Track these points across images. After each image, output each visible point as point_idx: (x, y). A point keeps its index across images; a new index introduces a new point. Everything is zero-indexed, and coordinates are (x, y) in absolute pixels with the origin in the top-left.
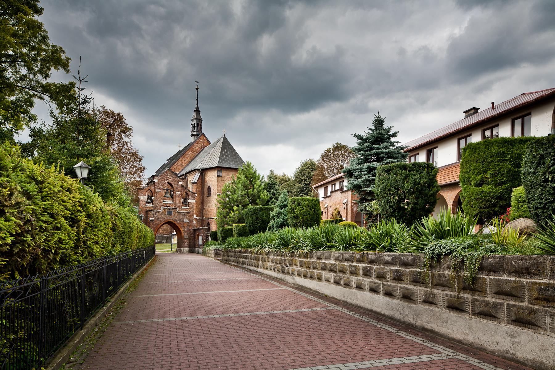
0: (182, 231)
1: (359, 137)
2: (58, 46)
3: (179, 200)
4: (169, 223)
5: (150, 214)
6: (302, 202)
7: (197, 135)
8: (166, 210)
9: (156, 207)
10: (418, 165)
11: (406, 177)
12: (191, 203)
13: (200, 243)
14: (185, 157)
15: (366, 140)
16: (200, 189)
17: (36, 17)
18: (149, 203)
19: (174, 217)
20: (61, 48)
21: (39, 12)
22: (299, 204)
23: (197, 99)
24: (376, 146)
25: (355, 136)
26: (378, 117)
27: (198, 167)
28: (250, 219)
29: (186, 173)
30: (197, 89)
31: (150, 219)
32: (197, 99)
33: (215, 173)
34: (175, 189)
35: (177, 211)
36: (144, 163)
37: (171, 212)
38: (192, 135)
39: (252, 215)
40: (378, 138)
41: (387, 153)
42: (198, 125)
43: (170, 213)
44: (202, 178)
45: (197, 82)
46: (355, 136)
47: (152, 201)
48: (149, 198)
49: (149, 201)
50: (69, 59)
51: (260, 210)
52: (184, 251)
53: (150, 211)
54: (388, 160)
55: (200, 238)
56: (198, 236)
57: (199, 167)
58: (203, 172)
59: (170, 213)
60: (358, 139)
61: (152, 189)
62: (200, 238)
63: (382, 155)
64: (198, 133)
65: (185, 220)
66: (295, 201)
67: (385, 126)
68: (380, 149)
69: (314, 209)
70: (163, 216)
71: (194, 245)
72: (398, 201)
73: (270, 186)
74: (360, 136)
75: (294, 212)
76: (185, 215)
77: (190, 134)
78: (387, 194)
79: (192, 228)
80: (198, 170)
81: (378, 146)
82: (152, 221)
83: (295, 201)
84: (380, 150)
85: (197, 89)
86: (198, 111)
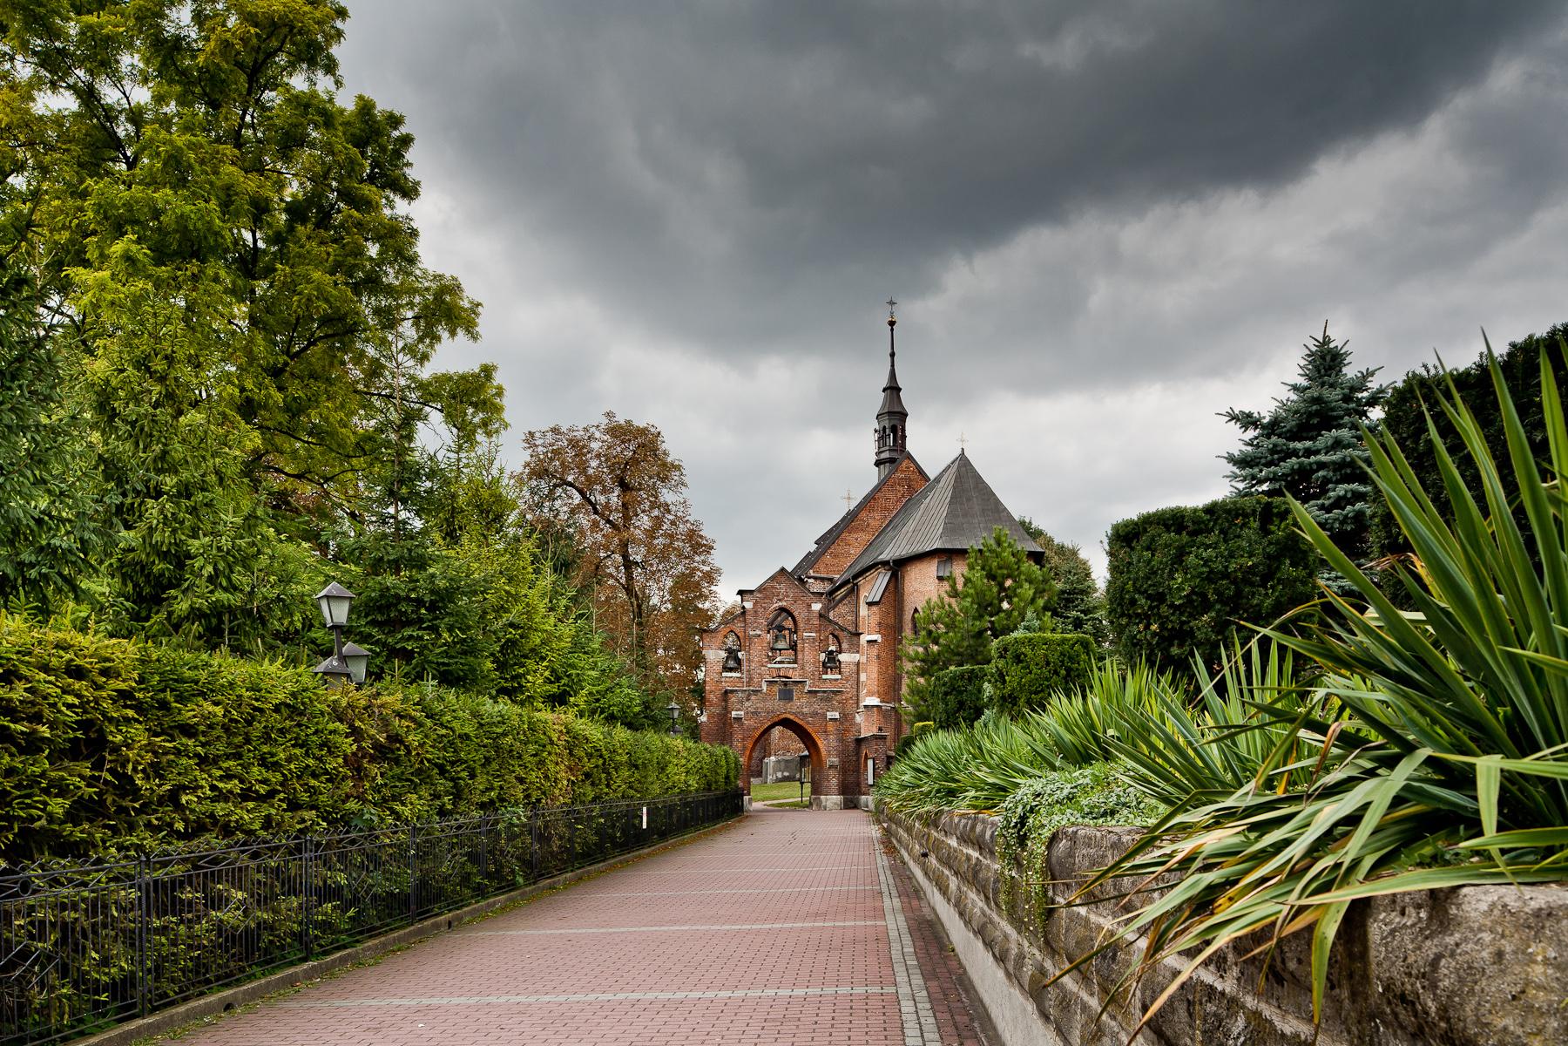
0: (821, 744)
1: (1247, 420)
2: (448, 275)
3: (811, 656)
4: (786, 723)
5: (733, 699)
6: (1027, 650)
7: (892, 461)
8: (776, 688)
9: (751, 679)
10: (1228, 512)
11: (1181, 554)
12: (849, 664)
13: (870, 781)
14: (857, 530)
15: (1272, 428)
16: (891, 621)
17: (401, 207)
18: (731, 670)
19: (800, 707)
20: (454, 279)
21: (409, 192)
22: (1018, 659)
23: (892, 355)
24: (1298, 445)
25: (1234, 417)
26: (1326, 340)
27: (883, 557)
28: (941, 706)
29: (856, 576)
30: (892, 324)
31: (734, 714)
32: (892, 355)
33: (930, 569)
34: (801, 625)
35: (807, 688)
36: (717, 558)
37: (791, 692)
38: (878, 463)
39: (946, 694)
40: (1311, 415)
41: (1339, 466)
42: (894, 429)
43: (787, 695)
44: (896, 587)
45: (892, 303)
46: (1234, 417)
47: (739, 661)
48: (732, 654)
49: (731, 664)
50: (479, 305)
51: (970, 679)
52: (829, 804)
53: (732, 691)
54: (1341, 489)
55: (870, 763)
56: (866, 758)
57: (887, 555)
58: (898, 567)
59: (787, 695)
60: (1245, 427)
61: (737, 630)
62: (870, 763)
63: (1320, 473)
64: (895, 455)
65: (830, 715)
66: (1006, 650)
67: (1350, 372)
68: (1317, 452)
69: (1069, 670)
70: (769, 705)
71: (858, 785)
72: (1162, 638)
73: (1068, 601)
74: (1249, 415)
75: (1004, 682)
76: (828, 700)
77: (874, 458)
78: (1129, 617)
79: (851, 737)
80: (885, 563)
81: (1308, 444)
82: (738, 719)
83: (1006, 650)
84: (1313, 459)
85: (892, 324)
86: (893, 389)
